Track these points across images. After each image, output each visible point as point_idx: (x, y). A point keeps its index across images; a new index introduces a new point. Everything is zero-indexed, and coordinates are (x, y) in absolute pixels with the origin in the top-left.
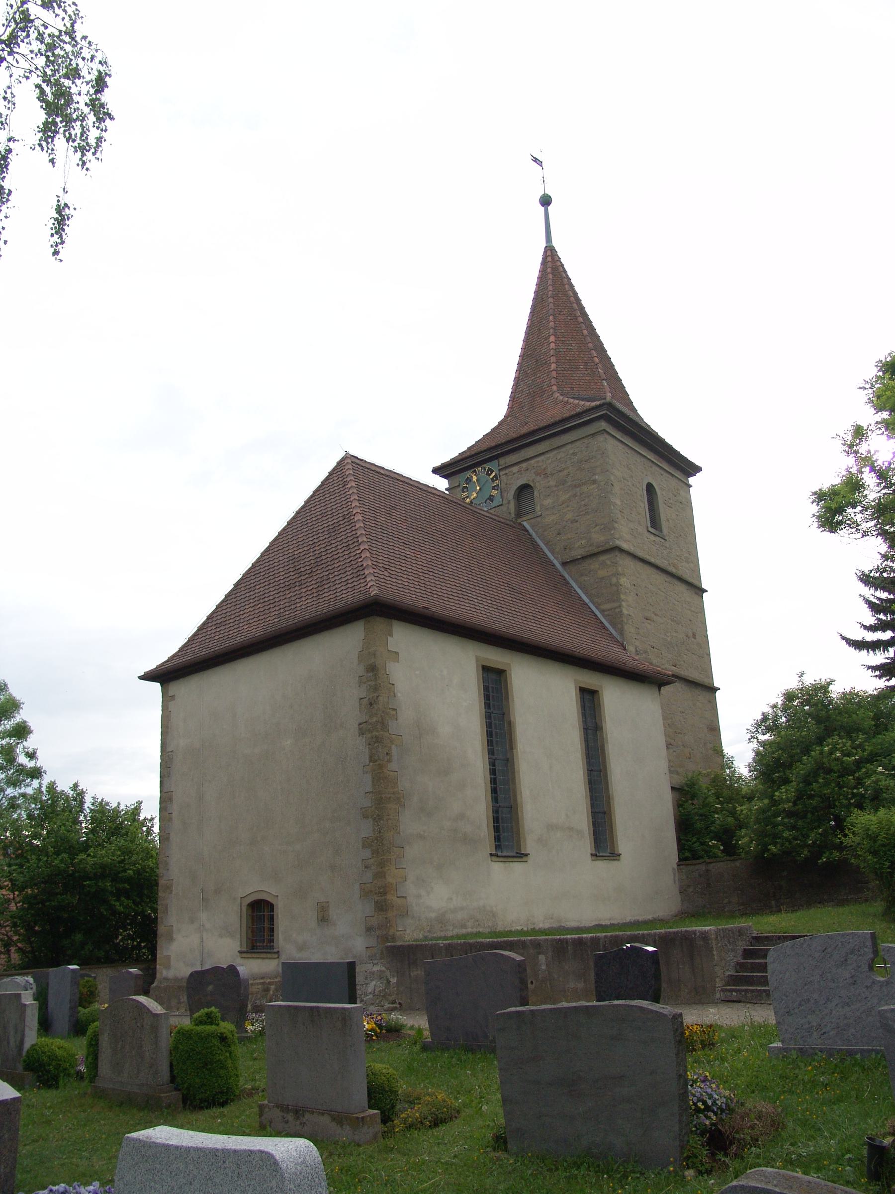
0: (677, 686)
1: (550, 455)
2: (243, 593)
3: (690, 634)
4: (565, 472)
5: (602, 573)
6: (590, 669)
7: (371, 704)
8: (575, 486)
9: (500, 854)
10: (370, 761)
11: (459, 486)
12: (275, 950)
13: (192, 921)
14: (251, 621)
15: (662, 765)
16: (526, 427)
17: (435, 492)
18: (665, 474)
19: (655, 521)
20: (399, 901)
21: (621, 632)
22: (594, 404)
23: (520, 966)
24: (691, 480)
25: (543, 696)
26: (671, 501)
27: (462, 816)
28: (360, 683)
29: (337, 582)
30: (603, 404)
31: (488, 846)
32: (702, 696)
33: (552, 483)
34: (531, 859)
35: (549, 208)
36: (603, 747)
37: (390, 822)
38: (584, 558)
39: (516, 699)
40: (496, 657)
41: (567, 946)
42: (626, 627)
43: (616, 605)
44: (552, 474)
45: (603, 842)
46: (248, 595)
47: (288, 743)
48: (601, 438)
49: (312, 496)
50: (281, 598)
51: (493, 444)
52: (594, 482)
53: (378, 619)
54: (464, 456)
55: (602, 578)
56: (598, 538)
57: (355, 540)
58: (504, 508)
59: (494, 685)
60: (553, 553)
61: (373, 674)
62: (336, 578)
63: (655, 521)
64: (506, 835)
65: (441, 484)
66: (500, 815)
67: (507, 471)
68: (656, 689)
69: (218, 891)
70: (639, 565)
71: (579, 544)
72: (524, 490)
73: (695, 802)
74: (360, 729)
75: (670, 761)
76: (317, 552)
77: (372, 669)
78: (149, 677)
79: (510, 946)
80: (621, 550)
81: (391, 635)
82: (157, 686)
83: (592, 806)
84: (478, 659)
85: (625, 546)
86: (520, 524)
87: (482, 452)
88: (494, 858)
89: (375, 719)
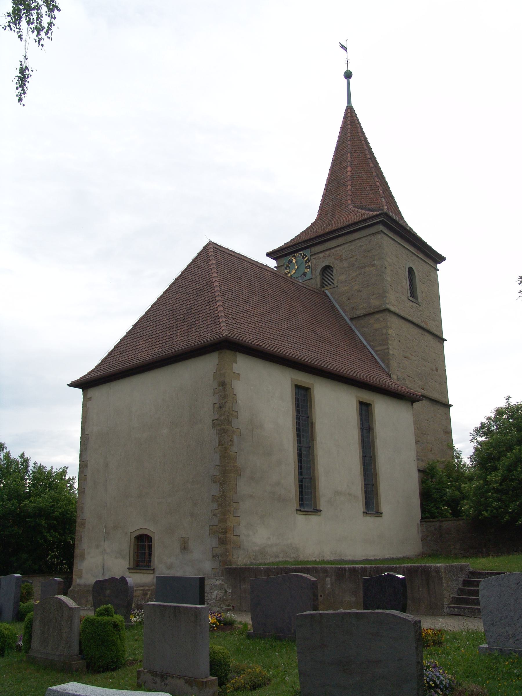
1: (345, 246)
5: (376, 326)
9: (302, 509)
11: (283, 265)
12: (152, 568)
14: (143, 350)
15: (413, 455)
16: (329, 227)
19: (413, 293)
20: (235, 538)
21: (388, 365)
22: (375, 213)
24: (439, 266)
31: (295, 503)
32: (441, 410)
35: (351, 80)
36: (373, 441)
38: (364, 315)
42: (391, 362)
43: (385, 347)
44: (346, 259)
45: (371, 504)
48: (379, 236)
49: (186, 269)
52: (373, 265)
53: (228, 352)
56: (375, 303)
57: (214, 299)
58: (313, 281)
59: (303, 398)
60: (344, 312)
61: (223, 387)
62: (201, 323)
63: (413, 293)
64: (307, 498)
65: (272, 263)
67: (316, 256)
70: (402, 321)
71: (361, 307)
72: (327, 269)
76: (189, 306)
77: (223, 384)
82: (79, 391)
84: (292, 380)
85: (393, 309)
86: (323, 292)
88: (299, 512)
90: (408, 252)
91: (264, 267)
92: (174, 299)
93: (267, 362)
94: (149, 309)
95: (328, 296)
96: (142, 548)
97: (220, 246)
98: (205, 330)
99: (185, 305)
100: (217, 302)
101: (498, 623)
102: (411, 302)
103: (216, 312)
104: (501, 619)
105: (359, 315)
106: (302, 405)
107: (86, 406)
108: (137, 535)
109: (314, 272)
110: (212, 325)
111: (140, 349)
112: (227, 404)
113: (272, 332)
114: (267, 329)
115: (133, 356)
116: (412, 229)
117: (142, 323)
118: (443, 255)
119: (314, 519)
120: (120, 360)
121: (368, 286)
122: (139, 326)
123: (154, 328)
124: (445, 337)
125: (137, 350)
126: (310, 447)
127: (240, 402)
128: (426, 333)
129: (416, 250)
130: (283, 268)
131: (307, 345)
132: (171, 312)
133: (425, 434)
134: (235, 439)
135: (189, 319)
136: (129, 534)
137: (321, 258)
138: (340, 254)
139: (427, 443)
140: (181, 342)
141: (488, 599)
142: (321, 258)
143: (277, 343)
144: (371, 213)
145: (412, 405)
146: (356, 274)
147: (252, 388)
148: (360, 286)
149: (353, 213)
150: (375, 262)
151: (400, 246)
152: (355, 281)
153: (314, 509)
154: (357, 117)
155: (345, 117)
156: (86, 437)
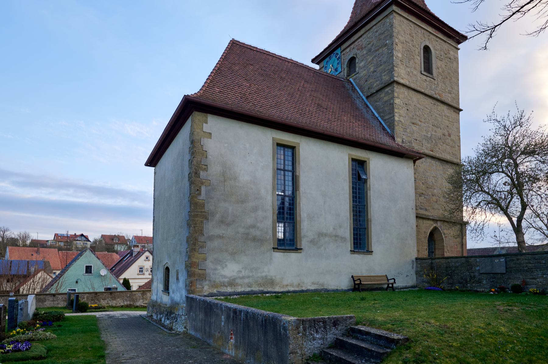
1: (365, 36)
3: (447, 134)
5: (386, 98)
15: (412, 204)
21: (393, 130)
24: (459, 46)
26: (442, 57)
27: (253, 226)
37: (197, 228)
38: (377, 91)
39: (302, 163)
42: (396, 128)
43: (392, 115)
44: (365, 47)
58: (342, 74)
60: (362, 93)
63: (428, 68)
65: (317, 67)
67: (344, 52)
68: (411, 163)
71: (375, 85)
72: (352, 60)
73: (35, 255)
80: (398, 83)
81: (206, 123)
84: (273, 139)
85: (402, 81)
88: (276, 250)
90: (425, 32)
93: (357, 149)
97: (254, 47)
119: (293, 256)
121: (381, 65)
124: (461, 107)
128: (439, 104)
129: (434, 30)
134: (203, 189)
151: (415, 26)
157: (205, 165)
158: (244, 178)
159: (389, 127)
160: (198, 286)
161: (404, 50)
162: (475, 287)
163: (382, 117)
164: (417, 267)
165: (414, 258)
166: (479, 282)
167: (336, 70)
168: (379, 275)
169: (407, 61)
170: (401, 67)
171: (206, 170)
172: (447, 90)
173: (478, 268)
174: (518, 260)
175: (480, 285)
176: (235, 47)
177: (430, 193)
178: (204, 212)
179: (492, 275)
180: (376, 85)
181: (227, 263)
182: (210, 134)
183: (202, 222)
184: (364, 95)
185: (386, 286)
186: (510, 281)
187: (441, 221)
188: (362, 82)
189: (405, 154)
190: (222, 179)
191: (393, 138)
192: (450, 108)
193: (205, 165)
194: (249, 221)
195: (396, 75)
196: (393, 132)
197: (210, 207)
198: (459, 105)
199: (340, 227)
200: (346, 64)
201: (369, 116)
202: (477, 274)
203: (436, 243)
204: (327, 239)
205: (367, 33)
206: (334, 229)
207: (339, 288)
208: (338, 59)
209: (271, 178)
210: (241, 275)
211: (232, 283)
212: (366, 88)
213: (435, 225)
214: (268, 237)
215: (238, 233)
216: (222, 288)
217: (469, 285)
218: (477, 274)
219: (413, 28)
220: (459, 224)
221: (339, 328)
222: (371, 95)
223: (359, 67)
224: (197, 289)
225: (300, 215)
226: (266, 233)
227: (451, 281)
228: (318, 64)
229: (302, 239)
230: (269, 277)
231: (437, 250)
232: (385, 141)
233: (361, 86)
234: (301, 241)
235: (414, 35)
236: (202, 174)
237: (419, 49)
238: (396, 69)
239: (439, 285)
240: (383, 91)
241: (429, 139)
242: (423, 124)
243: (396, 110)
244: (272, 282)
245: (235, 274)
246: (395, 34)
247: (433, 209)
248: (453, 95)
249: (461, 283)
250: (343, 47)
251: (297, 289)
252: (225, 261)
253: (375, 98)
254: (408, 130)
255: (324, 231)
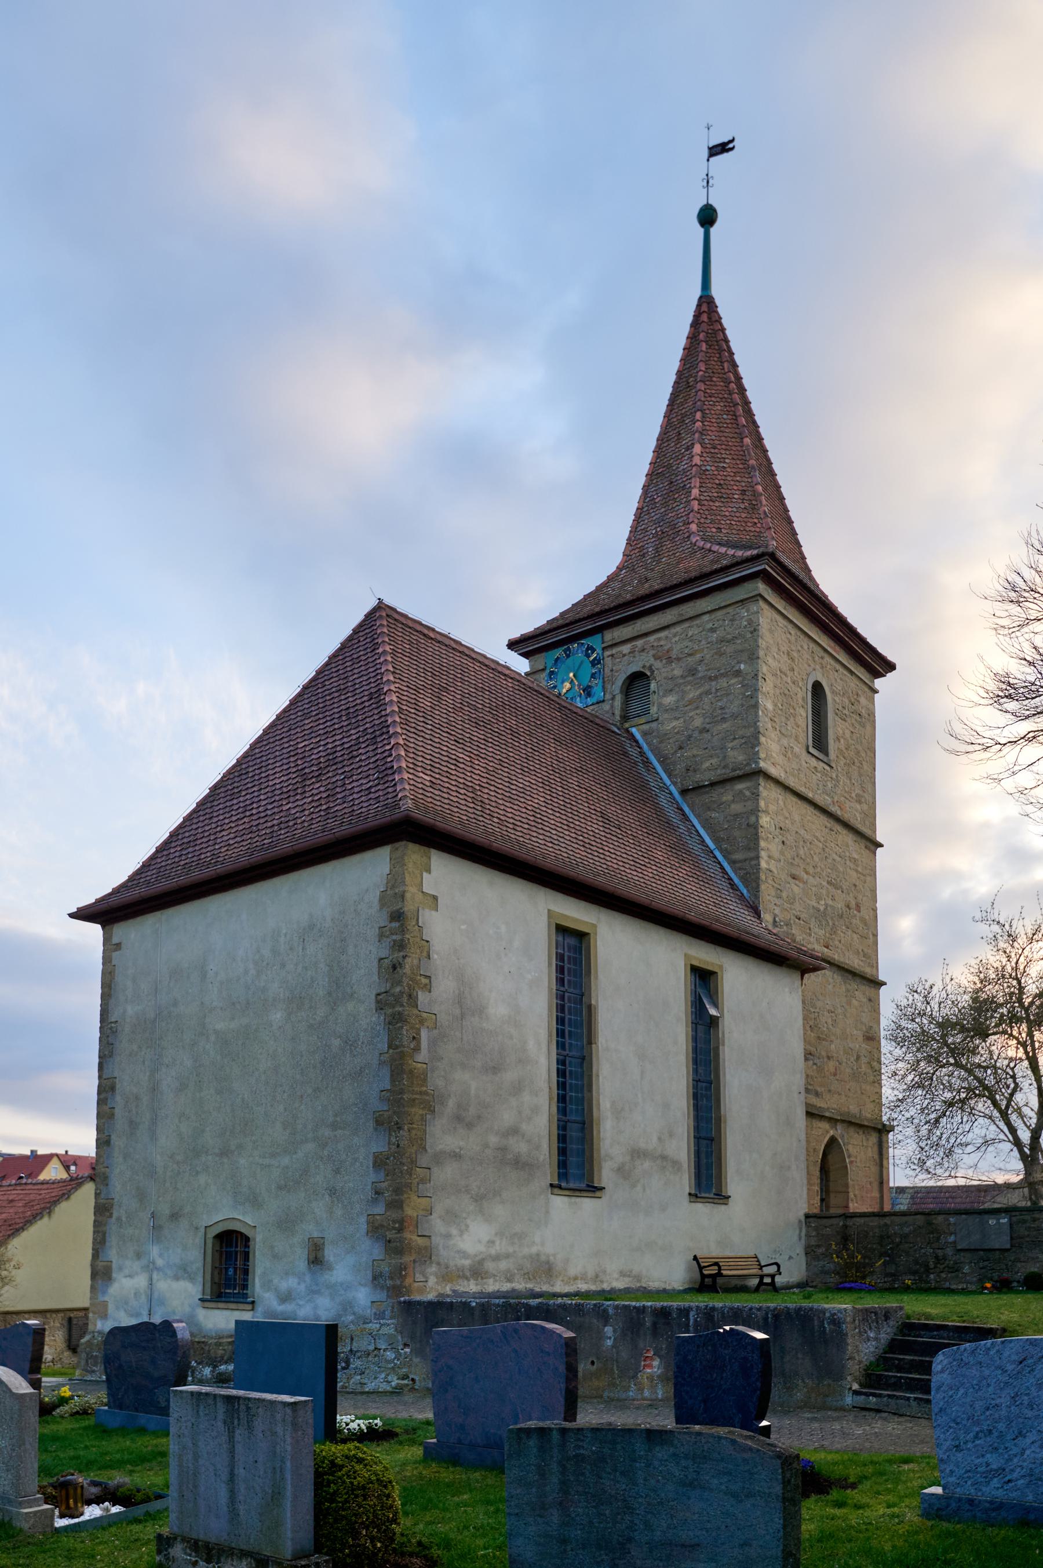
0: (828, 973)
1: (678, 629)
2: (222, 801)
3: (853, 904)
4: (698, 656)
5: (737, 808)
6: (708, 941)
7: (394, 967)
8: (710, 679)
9: (563, 1185)
10: (389, 1047)
11: (543, 670)
12: (249, 1300)
13: (138, 1256)
14: (231, 842)
16: (646, 585)
17: (507, 672)
18: (841, 670)
19: (820, 741)
20: (420, 1241)
21: (756, 891)
22: (748, 553)
23: (569, 1344)
24: (878, 683)
25: (639, 971)
26: (846, 712)
27: (514, 1131)
28: (381, 936)
29: (356, 790)
30: (763, 555)
31: (548, 1173)
32: (862, 992)
33: (677, 672)
34: (606, 1196)
35: (713, 230)
36: (717, 1049)
37: (414, 1132)
38: (713, 784)
39: (601, 976)
40: (577, 913)
41: (645, 1319)
42: (763, 887)
43: (752, 855)
45: (708, 1181)
46: (228, 804)
47: (277, 1016)
49: (327, 664)
50: (276, 810)
51: (597, 609)
53: (411, 845)
54: (555, 625)
55: (736, 815)
56: (737, 756)
57: (384, 730)
58: (606, 707)
59: (572, 953)
60: (669, 776)
61: (399, 923)
62: (355, 784)
63: (820, 741)
64: (575, 1164)
65: (521, 665)
66: (568, 1133)
67: (614, 651)
69: (175, 1216)
71: (707, 764)
72: (637, 680)
74: (378, 1002)
75: (807, 1076)
76: (330, 746)
77: (398, 916)
78: (84, 914)
79: (548, 1313)
80: (768, 777)
81: (429, 871)
82: (95, 931)
83: (697, 1128)
85: (773, 771)
86: (627, 731)
87: (580, 620)
88: (556, 1191)
89: (398, 989)
91: (500, 669)
92: (299, 730)
94: (246, 752)
95: (636, 741)
96: (230, 1260)
98: (363, 799)
99: (322, 743)
100: (390, 737)
101: (970, 1445)
102: (814, 759)
103: (389, 759)
104: (976, 1437)
105: (701, 784)
106: (569, 981)
107: (110, 962)
108: (230, 1228)
109: (608, 686)
110: (379, 787)
111: (226, 838)
112: (408, 960)
113: (509, 810)
114: (501, 802)
115: (209, 854)
116: (826, 597)
117: (230, 782)
118: (890, 658)
119: (587, 1204)
120: (182, 863)
122: (222, 790)
123: (256, 794)
124: (879, 838)
125: (219, 841)
126: (583, 1058)
127: (436, 956)
128: (838, 828)
129: (832, 644)
130: (544, 675)
131: (587, 841)
132: (292, 759)
133: (824, 1040)
134: (424, 1034)
135: (330, 774)
136: (203, 1230)
137: (624, 655)
138: (666, 648)
139: (829, 1058)
140: (309, 827)
141: (951, 1393)
142: (624, 655)
143: (520, 834)
144: (739, 553)
145: (802, 979)
146: (698, 693)
147: (463, 927)
148: (707, 720)
149: (704, 545)
150: (742, 666)
151: (799, 633)
152: (697, 708)
153: (588, 1186)
154: (721, 324)
155: (696, 324)
156: (111, 1028)
157: (426, 977)
158: (498, 1010)
159: (744, 879)
160: (419, 1277)
161: (778, 691)
162: (945, 1280)
163: (726, 854)
164: (808, 1236)
165: (801, 1215)
166: (955, 1269)
167: (588, 691)
168: (739, 1255)
169: (783, 719)
170: (773, 735)
171: (428, 988)
172: (853, 795)
173: (952, 1238)
174: (1034, 1220)
175: (957, 1276)
176: (381, 625)
177: (824, 1054)
178: (426, 1093)
179: (983, 1254)
180: (708, 769)
181: (468, 1221)
182: (435, 898)
183: (423, 1119)
184: (675, 784)
185: (755, 1282)
186: (1019, 1265)
187: (843, 1121)
188: (669, 748)
189: (788, 959)
190: (458, 1012)
191: (757, 914)
192: (859, 839)
193: (426, 977)
194: (507, 1117)
195: (762, 755)
196: (757, 897)
197: (436, 1082)
198: (875, 832)
199: (671, 1135)
200: (619, 683)
201: (697, 849)
202: (949, 1251)
203: (832, 1178)
204: (647, 1164)
205: (686, 625)
206: (660, 1139)
207: (668, 1288)
208: (594, 663)
209: (546, 1012)
210: (493, 1252)
211: (477, 1272)
212: (680, 767)
213: (832, 1133)
214: (541, 1158)
215: (486, 1146)
216: (460, 1281)
217: (932, 1276)
218: (949, 1251)
219: (793, 639)
220: (874, 1129)
221: (891, 1323)
222: (694, 789)
223: (660, 705)
224: (416, 1284)
225: (599, 1104)
226: (538, 1147)
227: (891, 1269)
228: (526, 655)
229: (603, 1164)
230: (543, 1258)
231: (832, 1195)
232: (735, 917)
233: (666, 758)
234: (600, 1170)
235: (795, 654)
236: (422, 997)
237: (804, 689)
238: (762, 739)
239: (864, 1277)
240: (728, 786)
241: (821, 916)
242: (811, 880)
243: (762, 844)
244: (547, 1269)
245: (481, 1248)
246: (761, 653)
247: (830, 1091)
248: (865, 807)
249: (914, 1273)
250: (610, 636)
251: (593, 1288)
252: (464, 1215)
253: (706, 798)
254: (784, 895)
255: (642, 1145)
